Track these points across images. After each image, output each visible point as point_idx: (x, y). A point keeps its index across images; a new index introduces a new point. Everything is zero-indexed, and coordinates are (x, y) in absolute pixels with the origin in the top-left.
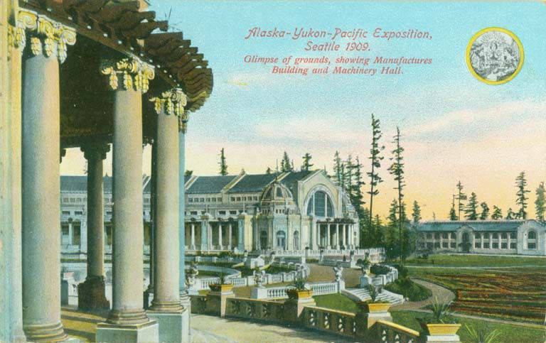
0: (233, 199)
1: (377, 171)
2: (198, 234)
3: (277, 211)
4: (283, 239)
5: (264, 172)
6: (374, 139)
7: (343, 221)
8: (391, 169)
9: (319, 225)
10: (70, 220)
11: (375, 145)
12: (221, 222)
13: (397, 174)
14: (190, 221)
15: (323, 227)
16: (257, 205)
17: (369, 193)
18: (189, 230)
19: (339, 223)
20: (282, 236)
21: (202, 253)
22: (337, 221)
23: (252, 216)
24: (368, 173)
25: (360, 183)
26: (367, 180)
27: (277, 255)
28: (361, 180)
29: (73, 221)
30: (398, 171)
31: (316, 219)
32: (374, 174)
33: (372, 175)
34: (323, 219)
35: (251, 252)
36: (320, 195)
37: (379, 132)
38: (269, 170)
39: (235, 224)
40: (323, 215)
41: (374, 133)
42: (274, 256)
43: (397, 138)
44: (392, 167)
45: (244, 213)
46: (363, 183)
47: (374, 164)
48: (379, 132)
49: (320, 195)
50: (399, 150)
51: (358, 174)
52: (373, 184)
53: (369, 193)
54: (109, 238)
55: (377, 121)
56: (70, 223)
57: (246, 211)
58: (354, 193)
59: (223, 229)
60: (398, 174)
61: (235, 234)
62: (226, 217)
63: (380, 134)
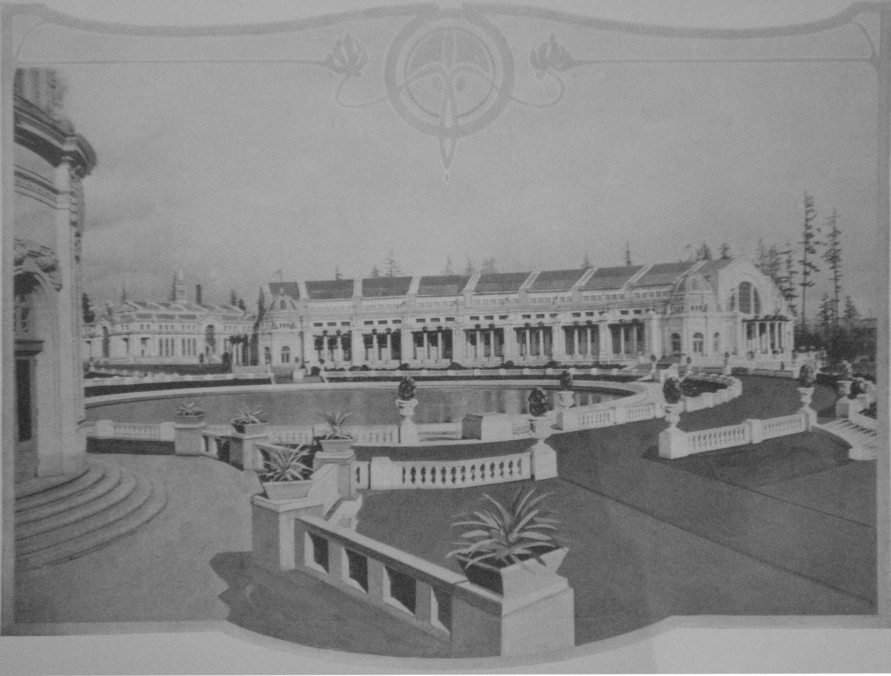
0: (638, 295)
1: (810, 258)
2: (501, 341)
3: (692, 307)
4: (701, 344)
5: (331, 277)
6: (807, 220)
7: (774, 318)
8: (826, 256)
9: (745, 324)
10: (478, 326)
11: (808, 227)
12: (576, 326)
13: (832, 263)
14: (537, 326)
15: (750, 324)
16: (666, 302)
17: (802, 284)
18: (584, 335)
19: (770, 320)
20: (699, 339)
21: (601, 363)
22: (767, 318)
23: (660, 316)
24: (800, 262)
25: (792, 273)
26: (799, 268)
27: (694, 363)
28: (793, 269)
29: (482, 327)
30: (834, 258)
31: (742, 316)
32: (807, 262)
33: (805, 263)
34: (750, 316)
35: (661, 361)
36: (745, 287)
37: (813, 211)
38: (375, 272)
39: (639, 326)
40: (748, 312)
41: (807, 212)
42: (690, 366)
43: (832, 219)
44: (827, 253)
45: (651, 312)
46: (796, 272)
47: (807, 249)
48: (813, 211)
49: (745, 287)
50: (835, 233)
51: (789, 261)
52: (806, 273)
53: (802, 284)
54: (345, 352)
55: (810, 199)
56: (491, 329)
57: (654, 310)
58: (786, 285)
59: (580, 335)
60: (834, 262)
61: (640, 337)
62: (583, 320)
63: (814, 213)
